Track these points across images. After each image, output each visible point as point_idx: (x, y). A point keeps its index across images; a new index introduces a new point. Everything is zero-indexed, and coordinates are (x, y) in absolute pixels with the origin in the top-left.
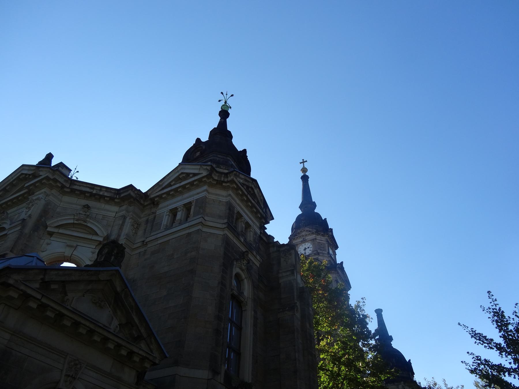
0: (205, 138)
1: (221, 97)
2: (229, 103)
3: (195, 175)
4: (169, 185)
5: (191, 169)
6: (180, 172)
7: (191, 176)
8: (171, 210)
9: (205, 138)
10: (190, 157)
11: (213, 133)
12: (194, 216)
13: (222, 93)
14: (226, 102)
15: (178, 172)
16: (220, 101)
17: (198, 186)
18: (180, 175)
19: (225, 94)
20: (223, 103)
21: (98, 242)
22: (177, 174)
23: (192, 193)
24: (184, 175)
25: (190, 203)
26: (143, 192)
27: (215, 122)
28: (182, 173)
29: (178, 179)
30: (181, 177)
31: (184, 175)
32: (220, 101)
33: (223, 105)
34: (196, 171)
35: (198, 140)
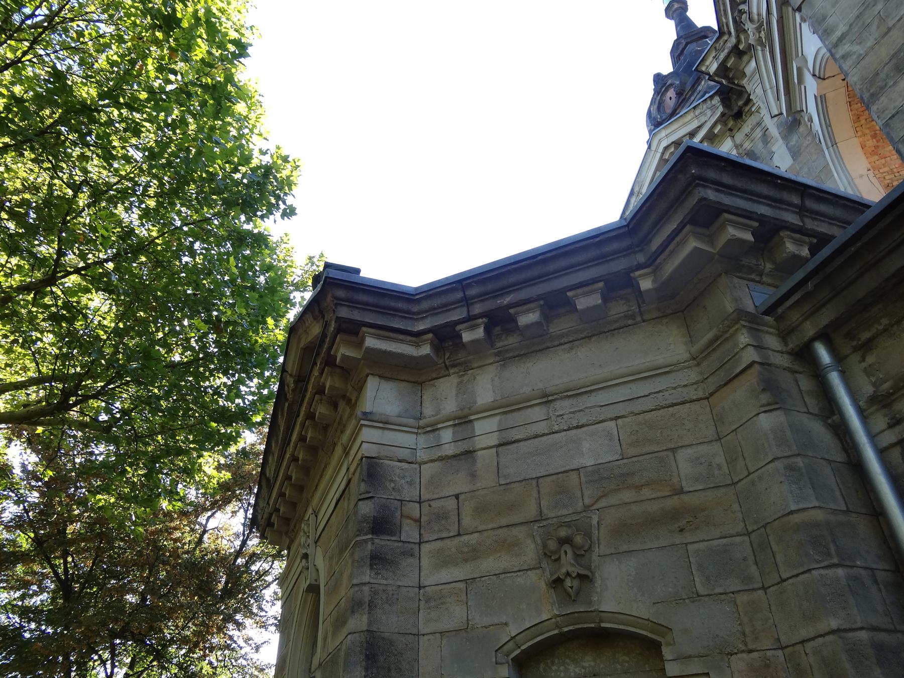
0: (667, 68)
6: (661, 150)
9: (667, 68)
10: (658, 118)
11: (677, 52)
15: (656, 151)
18: (663, 154)
22: (658, 155)
24: (672, 150)
28: (666, 148)
30: (666, 156)
31: (672, 150)
34: (694, 125)
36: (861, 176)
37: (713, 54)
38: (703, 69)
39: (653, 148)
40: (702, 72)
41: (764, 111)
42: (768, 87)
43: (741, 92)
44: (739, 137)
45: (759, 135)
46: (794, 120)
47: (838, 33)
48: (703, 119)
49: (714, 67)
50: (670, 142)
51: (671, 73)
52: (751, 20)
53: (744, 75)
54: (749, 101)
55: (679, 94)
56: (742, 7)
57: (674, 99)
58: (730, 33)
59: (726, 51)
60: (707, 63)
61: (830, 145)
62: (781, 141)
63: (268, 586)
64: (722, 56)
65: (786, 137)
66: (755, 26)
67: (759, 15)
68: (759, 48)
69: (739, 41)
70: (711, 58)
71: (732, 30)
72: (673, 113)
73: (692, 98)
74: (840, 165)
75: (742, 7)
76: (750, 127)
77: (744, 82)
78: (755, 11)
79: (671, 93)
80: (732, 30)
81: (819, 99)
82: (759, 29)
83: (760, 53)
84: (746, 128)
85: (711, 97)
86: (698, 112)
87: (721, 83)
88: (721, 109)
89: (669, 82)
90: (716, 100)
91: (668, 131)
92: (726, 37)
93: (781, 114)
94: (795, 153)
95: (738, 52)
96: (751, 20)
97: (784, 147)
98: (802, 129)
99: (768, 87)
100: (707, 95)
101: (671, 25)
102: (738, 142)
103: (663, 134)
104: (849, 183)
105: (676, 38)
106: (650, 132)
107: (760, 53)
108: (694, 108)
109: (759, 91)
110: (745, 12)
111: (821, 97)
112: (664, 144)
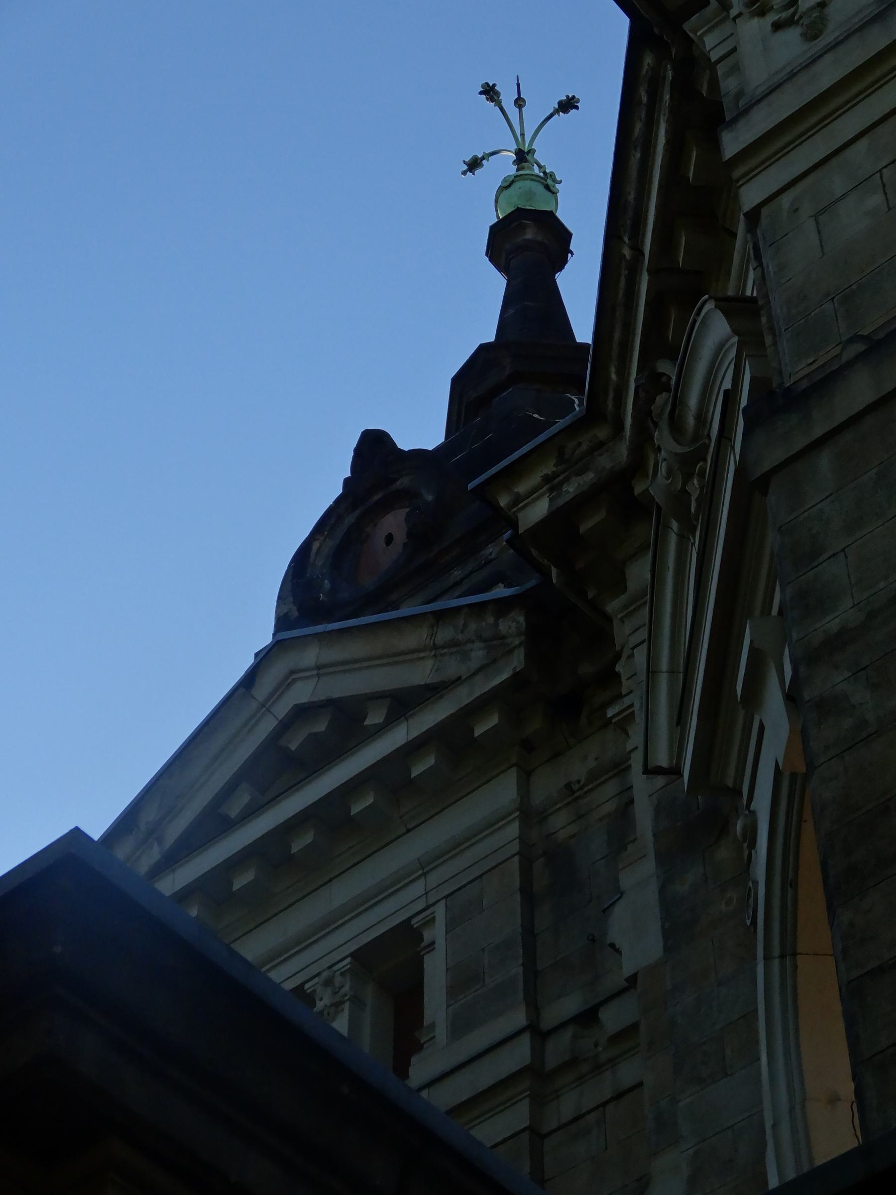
0: (422, 428)
1: (494, 134)
2: (546, 156)
3: (402, 703)
4: (214, 823)
5: (358, 666)
6: (283, 708)
7: (375, 718)
8: (364, 959)
9: (422, 428)
10: (324, 585)
11: (473, 387)
12: (460, 1026)
13: (490, 92)
14: (522, 157)
15: (266, 706)
16: (474, 165)
17: (441, 793)
18: (285, 726)
19: (508, 98)
20: (503, 166)
21: (526, 1039)
22: (267, 726)
23: (342, 892)
24: (321, 726)
25: (407, 938)
26: (492, 338)
27: (476, 306)
28: (302, 712)
29: (280, 764)
31: (321, 726)
32: (474, 165)
33: (507, 185)
34: (421, 673)
35: (374, 447)
36: (834, 1100)
37: (549, 468)
38: (503, 501)
39: (262, 690)
40: (496, 508)
41: (636, 738)
42: (664, 664)
43: (600, 636)
44: (547, 784)
45: (609, 807)
46: (705, 815)
47: (831, 623)
48: (453, 668)
49: (538, 510)
50: (321, 696)
51: (418, 454)
52: (676, 426)
53: (619, 584)
54: (609, 678)
55: (419, 537)
56: (666, 367)
57: (400, 537)
58: (619, 427)
59: (590, 476)
60: (522, 488)
61: (776, 951)
62: (649, 866)
63: (511, 651)
64: (571, 489)
65: (670, 858)
66: (679, 449)
67: (702, 418)
68: (675, 525)
69: (637, 465)
70: (535, 479)
71: (629, 421)
72: (379, 597)
73: (457, 574)
74: (786, 1038)
75: (666, 367)
76: (591, 763)
77: (613, 606)
78: (693, 401)
79: (394, 523)
80: (629, 421)
81: (786, 783)
82: (687, 464)
83: (673, 540)
84: (577, 766)
85: (502, 606)
86: (445, 634)
87: (547, 575)
88: (517, 661)
89: (404, 482)
90: (513, 624)
91: (356, 648)
92: (602, 433)
93: (675, 771)
94: (678, 926)
95: (620, 496)
96: (676, 426)
97: (653, 887)
98: (724, 853)
99: (664, 664)
100: (500, 591)
101: (494, 285)
102: (537, 799)
103: (310, 656)
104: (791, 1110)
105: (490, 336)
106: (282, 622)
107: (673, 540)
108: (440, 616)
109: (837, 621)
110: (669, 391)
111: (793, 775)
112: (302, 693)
